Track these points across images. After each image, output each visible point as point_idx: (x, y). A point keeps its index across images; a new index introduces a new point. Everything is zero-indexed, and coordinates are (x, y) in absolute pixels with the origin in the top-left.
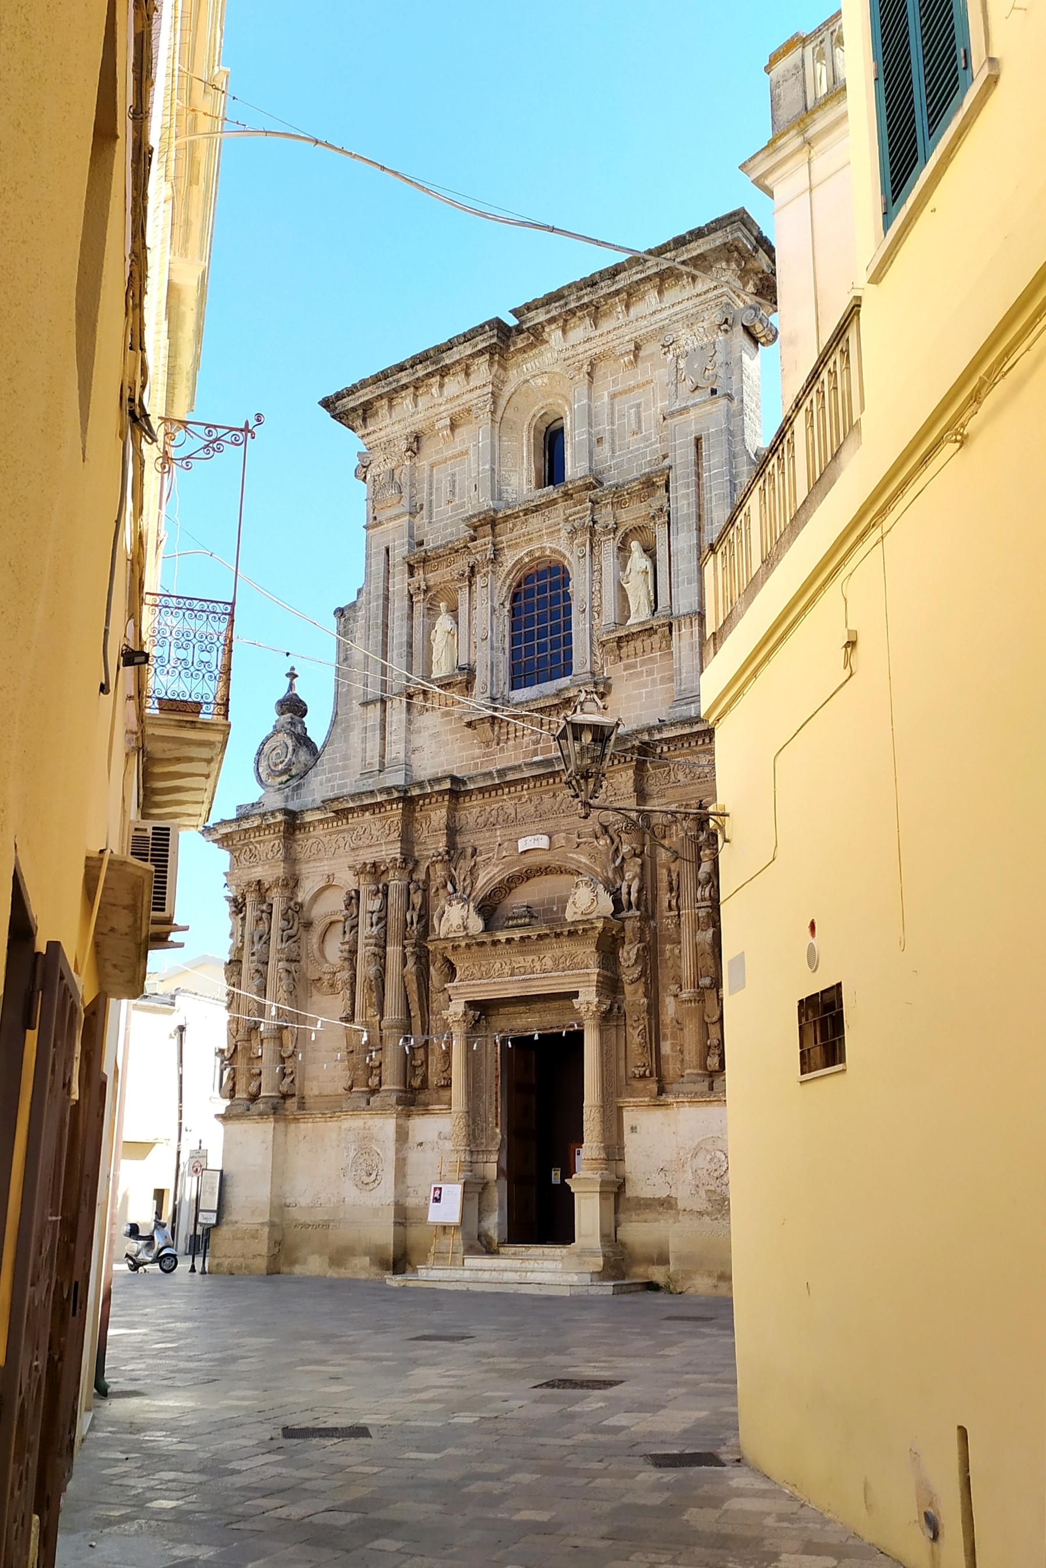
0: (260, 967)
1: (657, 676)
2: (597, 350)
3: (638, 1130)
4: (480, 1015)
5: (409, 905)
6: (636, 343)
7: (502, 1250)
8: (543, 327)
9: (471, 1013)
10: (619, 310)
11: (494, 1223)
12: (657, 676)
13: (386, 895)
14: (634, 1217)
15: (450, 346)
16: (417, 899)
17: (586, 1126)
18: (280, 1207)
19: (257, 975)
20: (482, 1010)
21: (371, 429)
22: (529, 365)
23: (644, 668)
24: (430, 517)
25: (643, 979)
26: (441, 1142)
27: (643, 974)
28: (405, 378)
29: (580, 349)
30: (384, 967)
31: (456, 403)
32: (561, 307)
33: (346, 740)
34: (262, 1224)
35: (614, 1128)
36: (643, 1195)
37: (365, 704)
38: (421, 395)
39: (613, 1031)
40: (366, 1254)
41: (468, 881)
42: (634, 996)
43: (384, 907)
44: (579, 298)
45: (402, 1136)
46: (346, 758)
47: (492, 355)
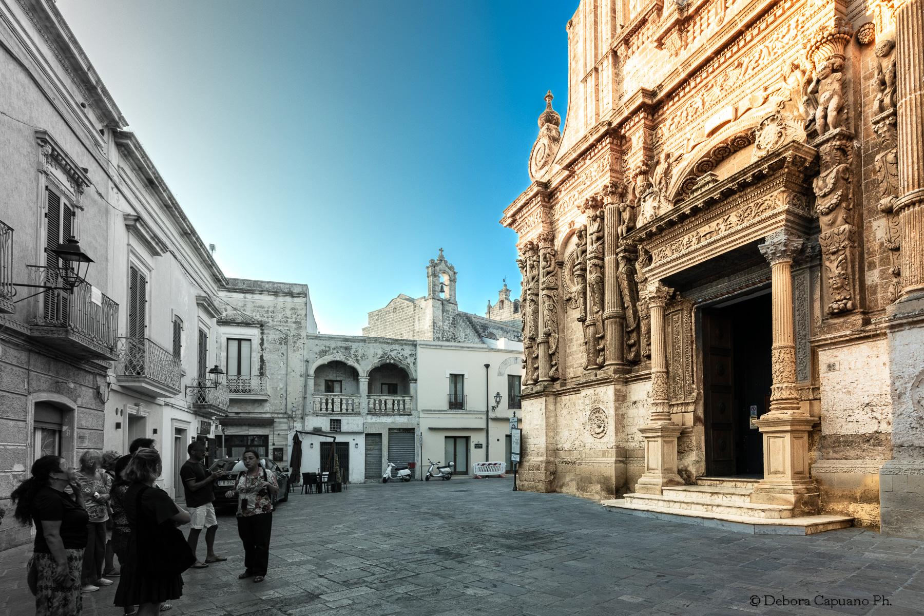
0: (534, 298)
3: (837, 367)
4: (674, 293)
5: (620, 221)
7: (699, 482)
9: (666, 289)
11: (694, 460)
13: (603, 219)
14: (831, 454)
16: (626, 216)
17: (776, 367)
18: (553, 451)
19: (532, 304)
25: (844, 205)
27: (844, 198)
30: (603, 274)
34: (541, 462)
35: (808, 370)
36: (843, 432)
39: (807, 276)
40: (598, 483)
41: (663, 182)
42: (833, 229)
43: (601, 229)
45: (621, 398)
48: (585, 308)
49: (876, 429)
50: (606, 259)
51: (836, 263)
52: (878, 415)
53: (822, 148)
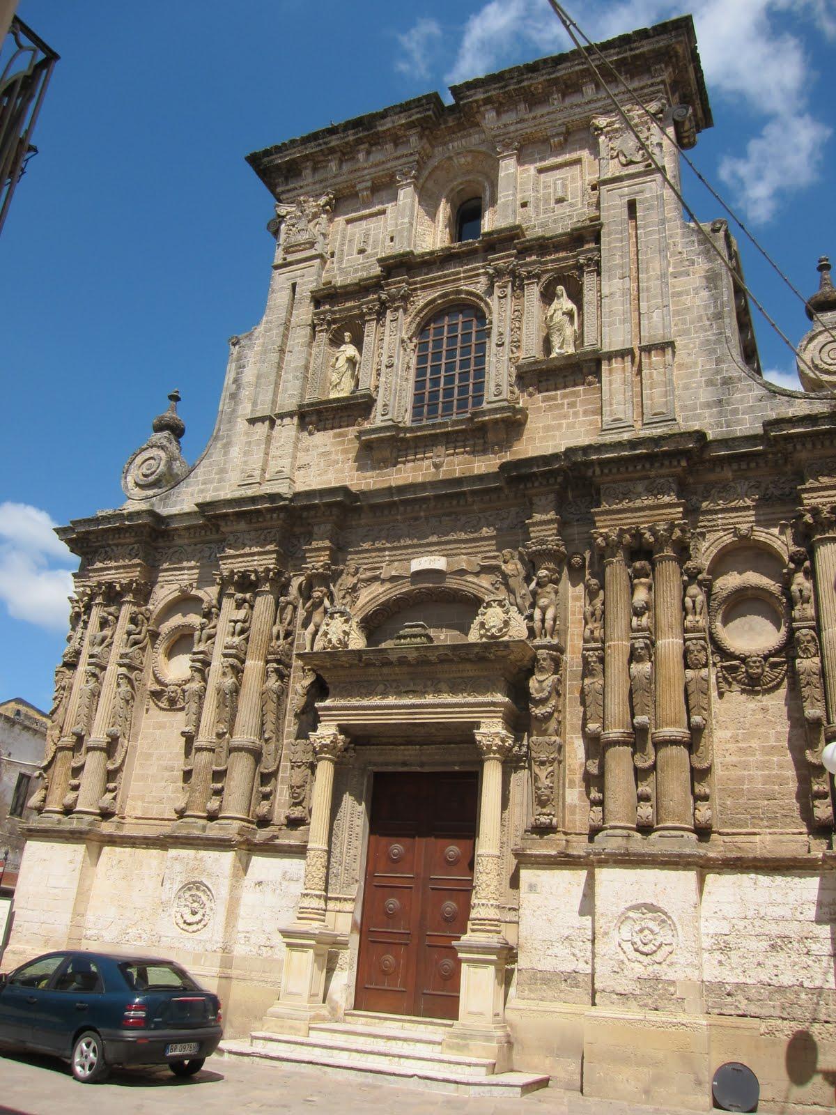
1: (580, 409)
2: (528, 131)
6: (567, 129)
7: (349, 1018)
8: (478, 107)
10: (555, 96)
12: (580, 409)
15: (383, 115)
20: (357, 737)
21: (292, 186)
22: (455, 144)
23: (566, 401)
24: (340, 262)
26: (285, 883)
28: (334, 141)
29: (512, 128)
31: (381, 168)
32: (501, 88)
33: (226, 454)
37: (252, 421)
38: (347, 160)
44: (519, 82)
46: (222, 471)
47: (424, 129)
48: (199, 720)
49: (573, 967)
50: (249, 663)
51: (545, 774)
52: (577, 952)
53: (540, 651)
